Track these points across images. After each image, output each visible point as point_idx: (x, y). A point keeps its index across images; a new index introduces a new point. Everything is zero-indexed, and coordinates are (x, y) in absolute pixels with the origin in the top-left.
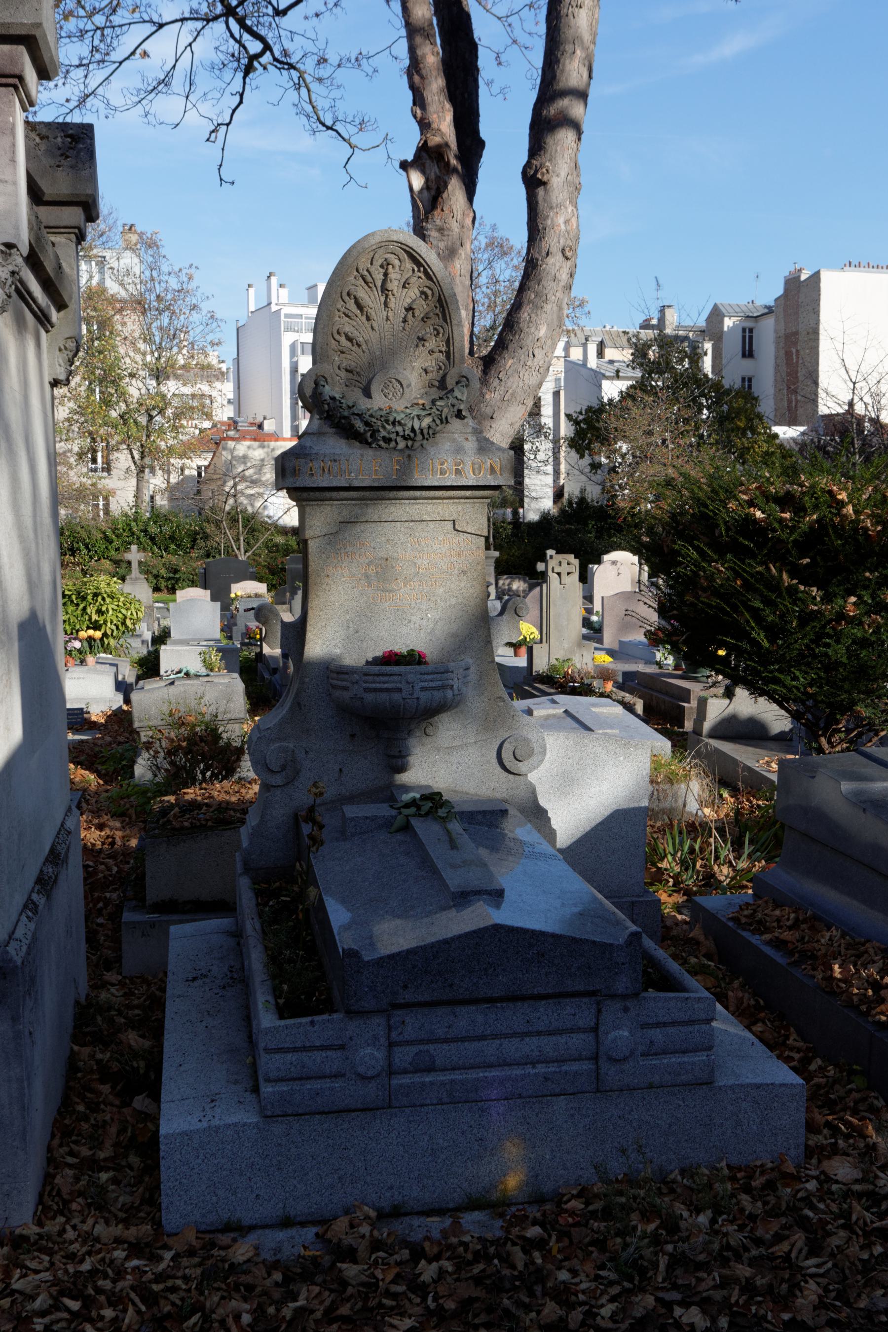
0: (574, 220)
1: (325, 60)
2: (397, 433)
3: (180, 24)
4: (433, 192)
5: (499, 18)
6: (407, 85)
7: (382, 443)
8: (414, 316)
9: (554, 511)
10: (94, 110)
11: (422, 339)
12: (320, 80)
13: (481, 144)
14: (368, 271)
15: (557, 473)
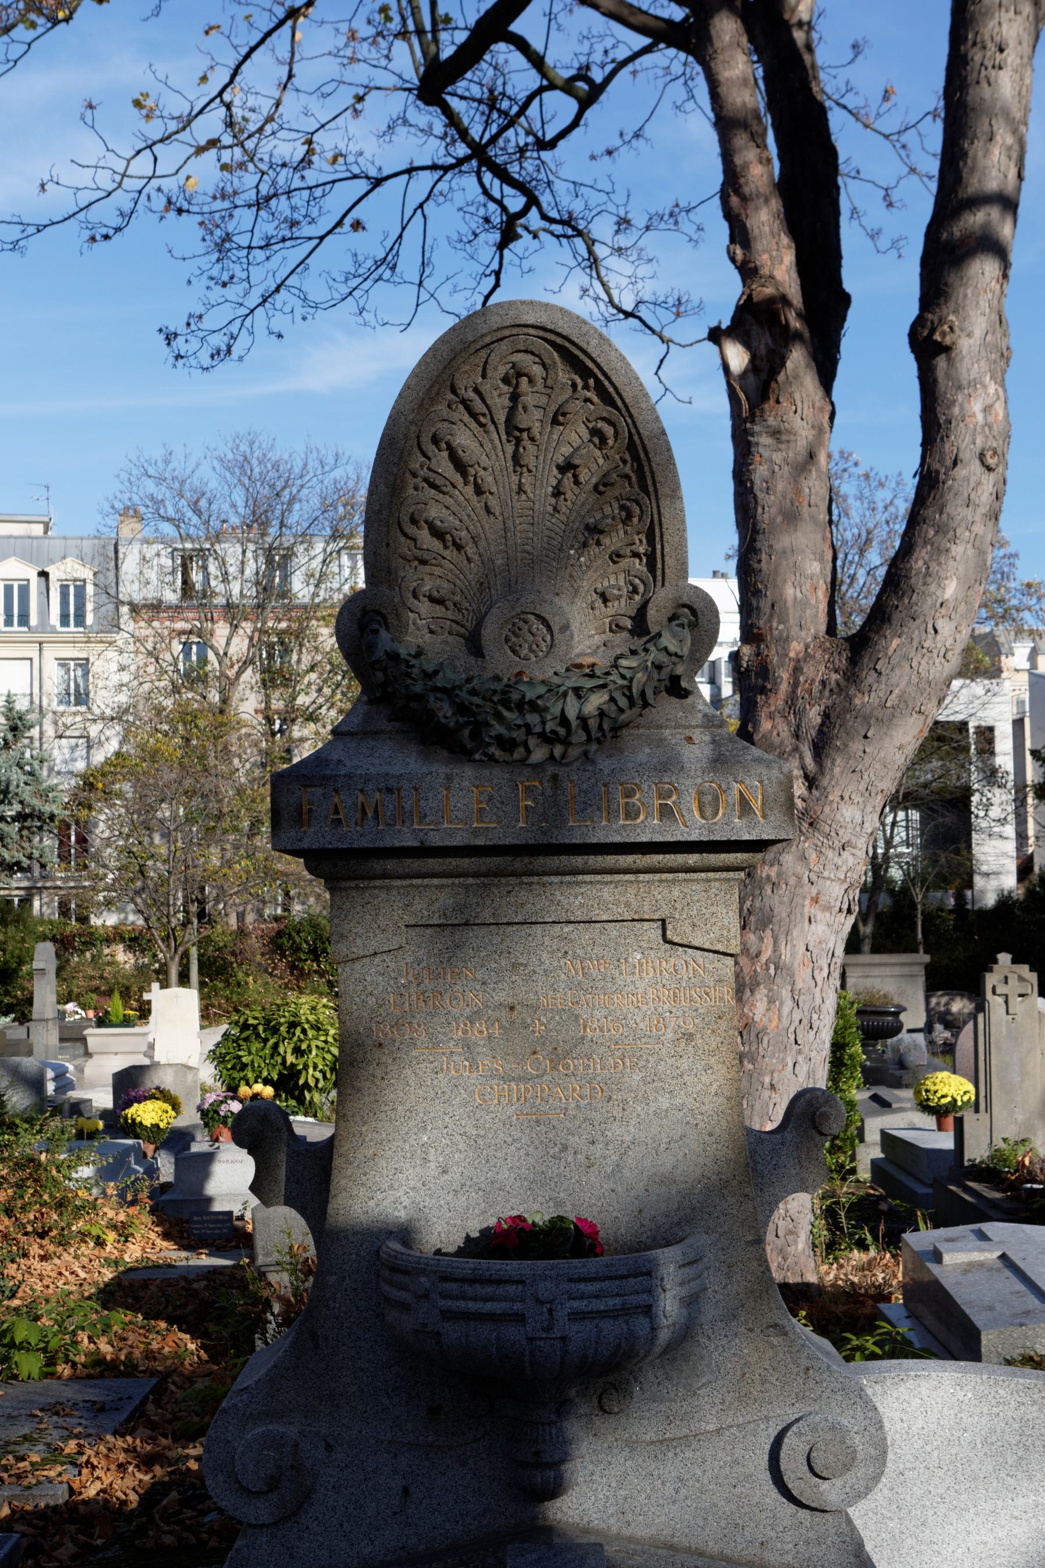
0: (999, 407)
2: (528, 726)
3: (406, 177)
4: (764, 376)
5: (887, 137)
6: (721, 214)
8: (577, 482)
9: (1020, 893)
10: (288, 309)
11: (595, 531)
12: (619, 251)
13: (845, 300)
14: (476, 390)
15: (1021, 837)
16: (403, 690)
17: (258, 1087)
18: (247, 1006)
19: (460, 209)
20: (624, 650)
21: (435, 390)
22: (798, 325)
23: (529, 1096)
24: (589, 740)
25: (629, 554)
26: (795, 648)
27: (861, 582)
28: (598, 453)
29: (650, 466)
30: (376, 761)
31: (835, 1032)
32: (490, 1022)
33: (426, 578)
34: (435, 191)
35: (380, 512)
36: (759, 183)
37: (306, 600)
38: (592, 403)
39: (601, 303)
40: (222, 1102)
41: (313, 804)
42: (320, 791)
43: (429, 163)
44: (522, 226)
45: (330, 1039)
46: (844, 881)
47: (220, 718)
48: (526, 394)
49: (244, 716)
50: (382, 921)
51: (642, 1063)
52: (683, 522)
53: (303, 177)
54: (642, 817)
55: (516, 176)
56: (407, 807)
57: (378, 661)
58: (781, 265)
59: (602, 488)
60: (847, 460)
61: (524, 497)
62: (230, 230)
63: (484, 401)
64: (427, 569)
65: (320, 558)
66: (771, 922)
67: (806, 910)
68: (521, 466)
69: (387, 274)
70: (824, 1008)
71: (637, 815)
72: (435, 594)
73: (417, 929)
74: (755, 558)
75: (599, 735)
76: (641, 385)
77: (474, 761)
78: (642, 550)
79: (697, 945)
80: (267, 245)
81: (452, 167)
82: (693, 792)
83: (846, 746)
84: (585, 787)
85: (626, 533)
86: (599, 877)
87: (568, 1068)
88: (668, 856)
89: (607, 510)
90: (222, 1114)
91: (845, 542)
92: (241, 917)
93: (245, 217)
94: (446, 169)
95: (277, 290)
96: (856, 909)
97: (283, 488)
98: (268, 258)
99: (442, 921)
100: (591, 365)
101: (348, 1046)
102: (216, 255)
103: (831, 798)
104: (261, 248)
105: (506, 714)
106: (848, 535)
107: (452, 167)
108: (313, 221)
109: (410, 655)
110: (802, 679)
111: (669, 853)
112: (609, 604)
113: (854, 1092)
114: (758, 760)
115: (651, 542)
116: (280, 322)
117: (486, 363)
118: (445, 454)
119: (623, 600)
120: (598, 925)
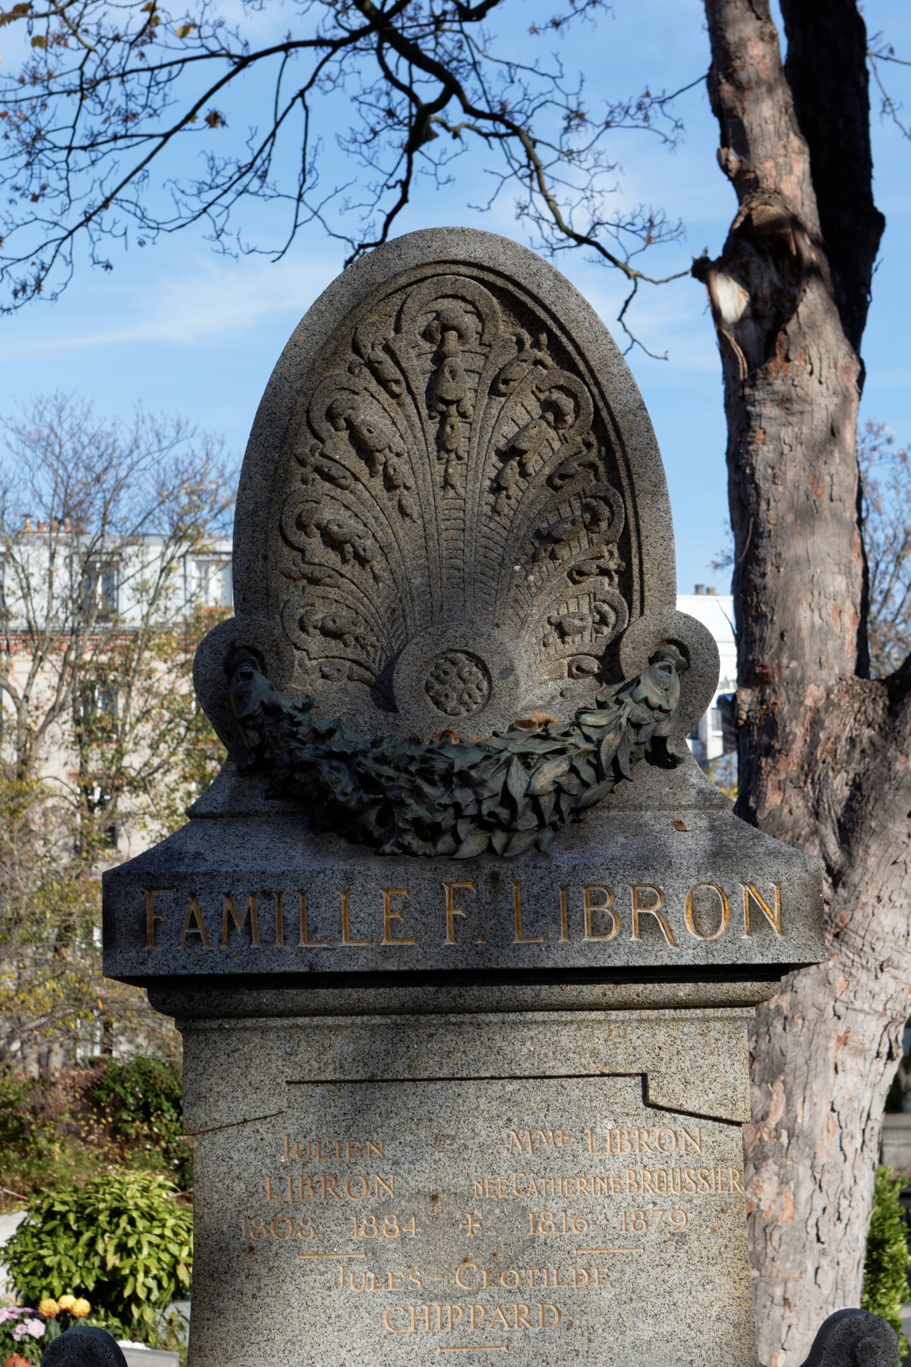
1: (580, 116)
2: (457, 806)
3: (281, 55)
4: (768, 325)
6: (709, 108)
7: (409, 839)
8: (524, 474)
10: (118, 230)
11: (548, 540)
13: (877, 222)
14: (387, 349)
16: (286, 757)
17: (68, 1301)
18: (51, 1185)
19: (355, 99)
20: (589, 701)
21: (331, 348)
22: (814, 256)
23: (457, 1321)
24: (542, 825)
25: (595, 571)
26: (813, 694)
27: (898, 600)
28: (552, 433)
29: (624, 452)
30: (249, 855)
31: (872, 1224)
32: (404, 1218)
33: (318, 603)
34: (321, 74)
35: (255, 512)
36: (761, 67)
37: (138, 623)
38: (545, 367)
39: (545, 225)
40: (17, 1322)
41: (160, 913)
42: (170, 895)
43: (313, 37)
44: (437, 121)
45: (168, 1233)
46: (883, 1014)
47: (18, 785)
48: (455, 354)
49: (50, 782)
50: (255, 1076)
51: (614, 1275)
52: (669, 527)
53: (142, 55)
54: (614, 932)
55: (431, 55)
56: (291, 918)
57: (251, 717)
58: (790, 176)
59: (558, 482)
60: (877, 434)
61: (451, 493)
62: (43, 124)
63: (397, 363)
64: (320, 590)
65: (157, 565)
66: (782, 1071)
67: (831, 1054)
68: (449, 452)
69: (255, 185)
70: (857, 1192)
71: (608, 929)
72: (330, 625)
73: (304, 1087)
74: (757, 570)
75: (555, 818)
76: (611, 342)
77: (384, 854)
78: (612, 565)
79: (691, 1109)
80: (92, 145)
81: (343, 42)
82: (684, 897)
83: (884, 827)
84: (535, 890)
85: (591, 542)
86: (554, 1015)
87: (512, 1282)
88: (650, 986)
89: (566, 511)
90: (17, 1338)
91: (875, 545)
92: (43, 1060)
93: (63, 109)
94: (335, 45)
95: (105, 204)
96: (900, 1053)
97: (106, 470)
98: (93, 163)
99: (338, 1076)
100: (543, 315)
101: (206, 1250)
102: (24, 158)
103: (863, 899)
104: (84, 148)
105: (427, 789)
106: (880, 537)
107: (343, 42)
108: (155, 113)
109: (295, 708)
110: (822, 735)
111: (652, 981)
112: (568, 639)
113: (897, 1307)
114: (773, 854)
115: (625, 554)
116: (108, 248)
117: (400, 312)
118: (345, 434)
119: (587, 635)
120: (553, 1082)
